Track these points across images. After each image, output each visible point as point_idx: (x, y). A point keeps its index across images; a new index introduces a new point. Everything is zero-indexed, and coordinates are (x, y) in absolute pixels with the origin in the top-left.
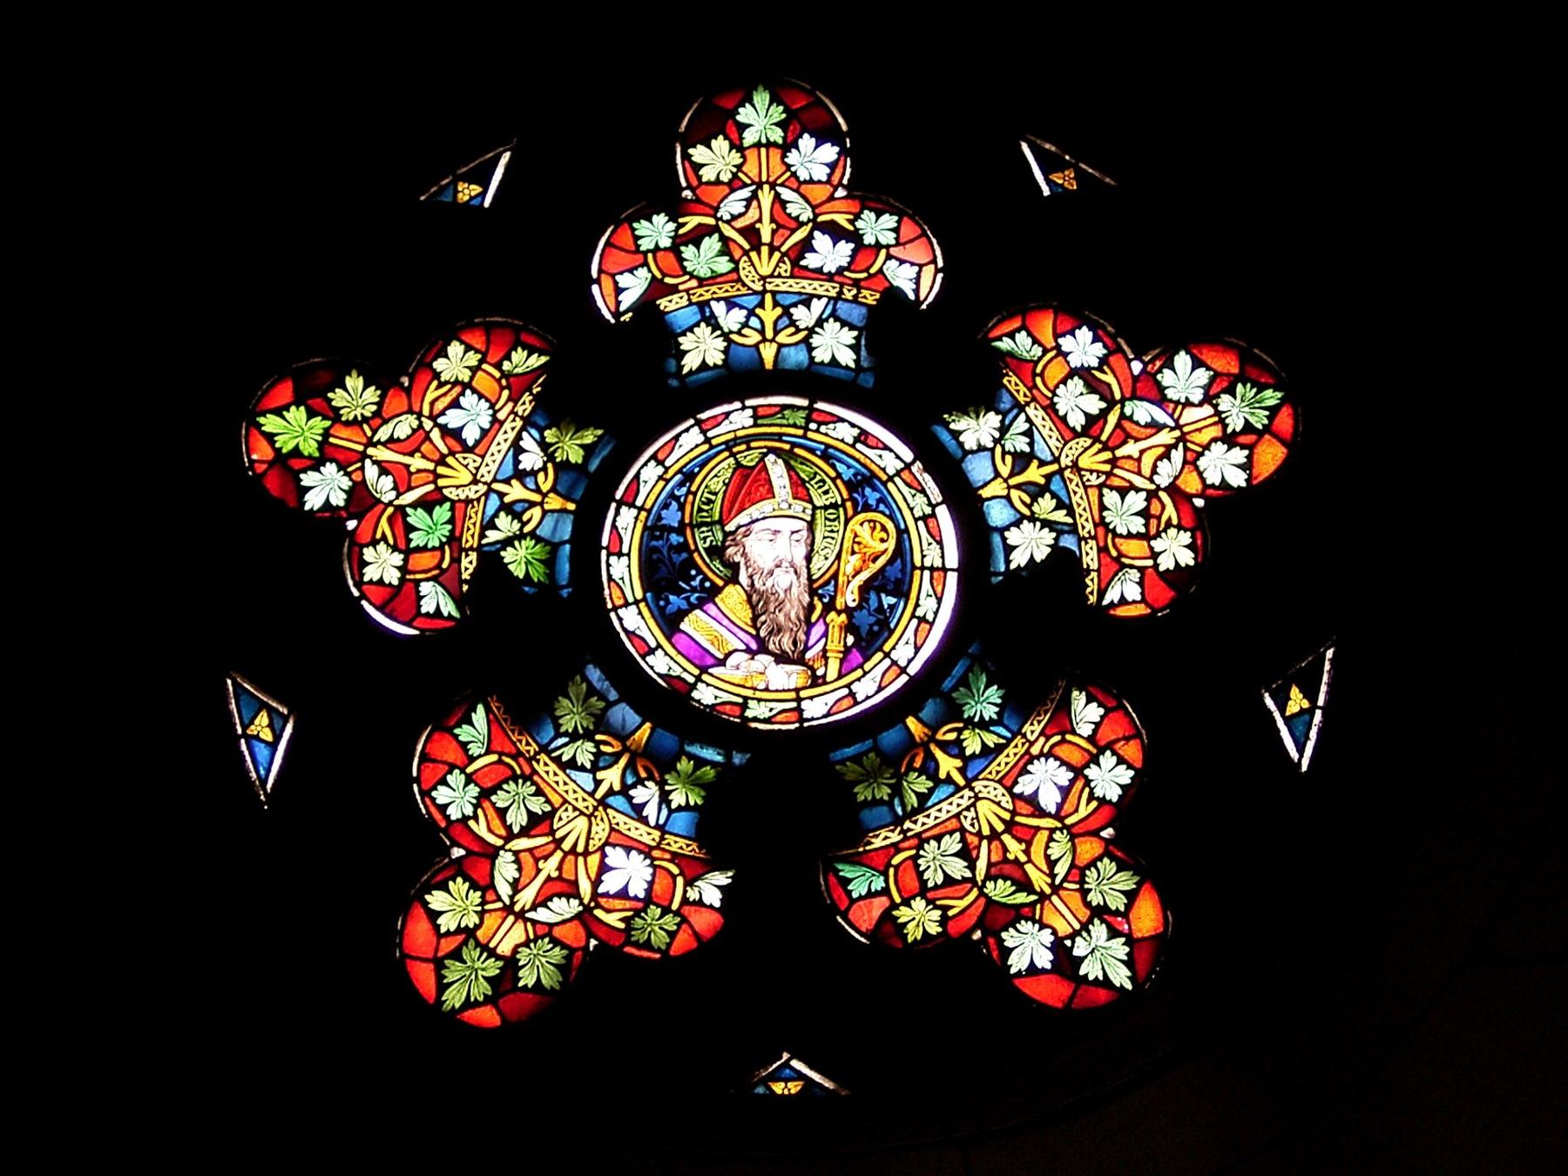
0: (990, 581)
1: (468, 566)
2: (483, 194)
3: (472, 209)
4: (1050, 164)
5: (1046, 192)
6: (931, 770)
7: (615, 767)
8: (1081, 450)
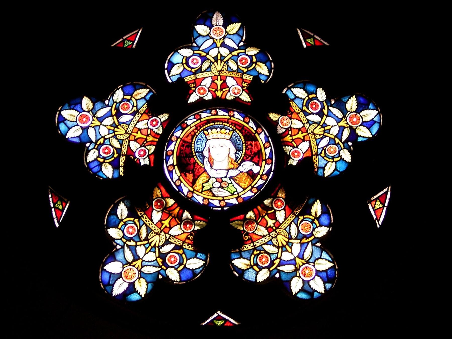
0: (276, 278)
1: (123, 160)
2: (133, 44)
3: (129, 49)
4: (306, 37)
5: (305, 46)
6: (261, 268)
7: (167, 220)
8: (314, 128)
